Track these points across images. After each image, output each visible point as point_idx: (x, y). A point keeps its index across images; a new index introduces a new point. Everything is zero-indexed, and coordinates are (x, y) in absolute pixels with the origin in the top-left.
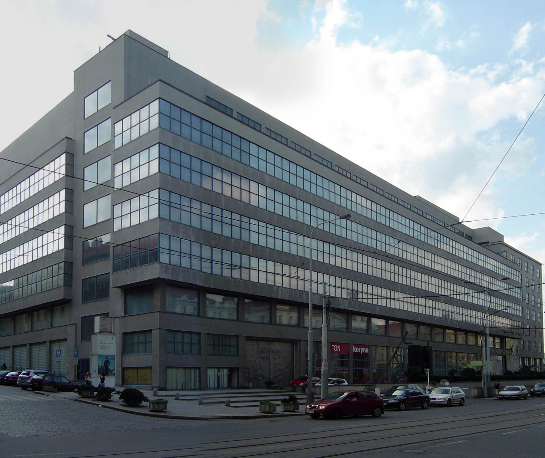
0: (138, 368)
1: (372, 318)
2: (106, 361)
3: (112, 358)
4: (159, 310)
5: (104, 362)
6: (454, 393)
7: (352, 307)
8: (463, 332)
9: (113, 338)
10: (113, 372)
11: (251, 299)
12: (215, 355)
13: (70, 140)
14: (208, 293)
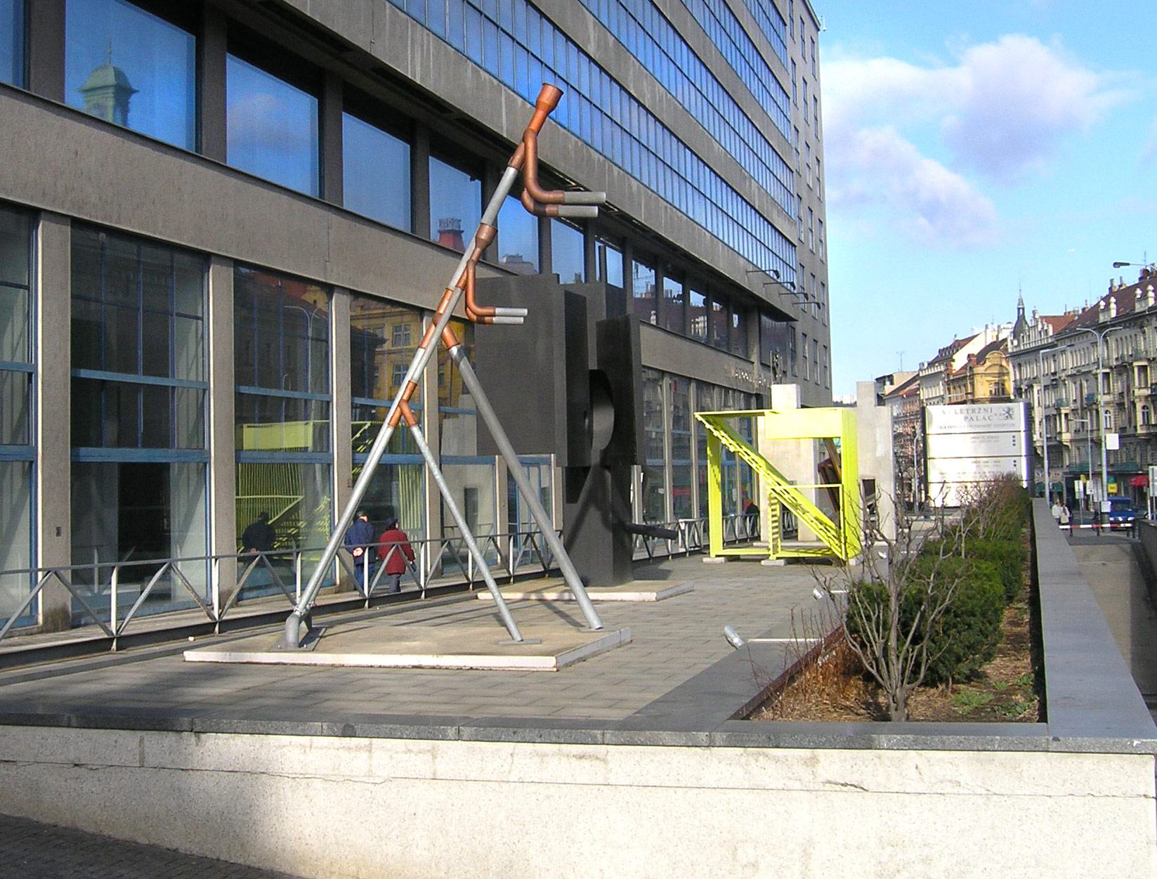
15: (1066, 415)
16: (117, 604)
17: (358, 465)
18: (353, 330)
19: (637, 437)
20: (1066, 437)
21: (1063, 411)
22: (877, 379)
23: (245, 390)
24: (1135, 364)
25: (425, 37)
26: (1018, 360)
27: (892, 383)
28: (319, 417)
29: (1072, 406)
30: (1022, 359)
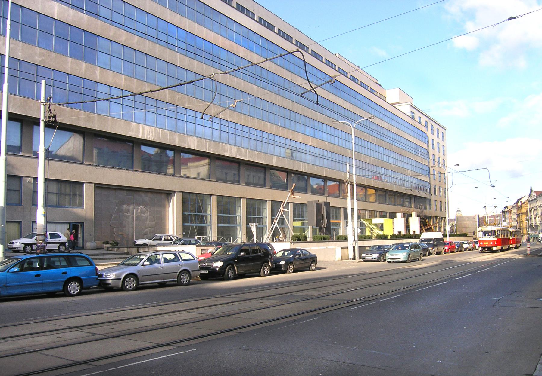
1: (311, 178)
14: (142, 145)
15: (538, 217)
16: (274, 229)
22: (505, 207)
25: (415, 135)
27: (507, 209)
28: (368, 217)
29: (540, 215)
30: (531, 202)
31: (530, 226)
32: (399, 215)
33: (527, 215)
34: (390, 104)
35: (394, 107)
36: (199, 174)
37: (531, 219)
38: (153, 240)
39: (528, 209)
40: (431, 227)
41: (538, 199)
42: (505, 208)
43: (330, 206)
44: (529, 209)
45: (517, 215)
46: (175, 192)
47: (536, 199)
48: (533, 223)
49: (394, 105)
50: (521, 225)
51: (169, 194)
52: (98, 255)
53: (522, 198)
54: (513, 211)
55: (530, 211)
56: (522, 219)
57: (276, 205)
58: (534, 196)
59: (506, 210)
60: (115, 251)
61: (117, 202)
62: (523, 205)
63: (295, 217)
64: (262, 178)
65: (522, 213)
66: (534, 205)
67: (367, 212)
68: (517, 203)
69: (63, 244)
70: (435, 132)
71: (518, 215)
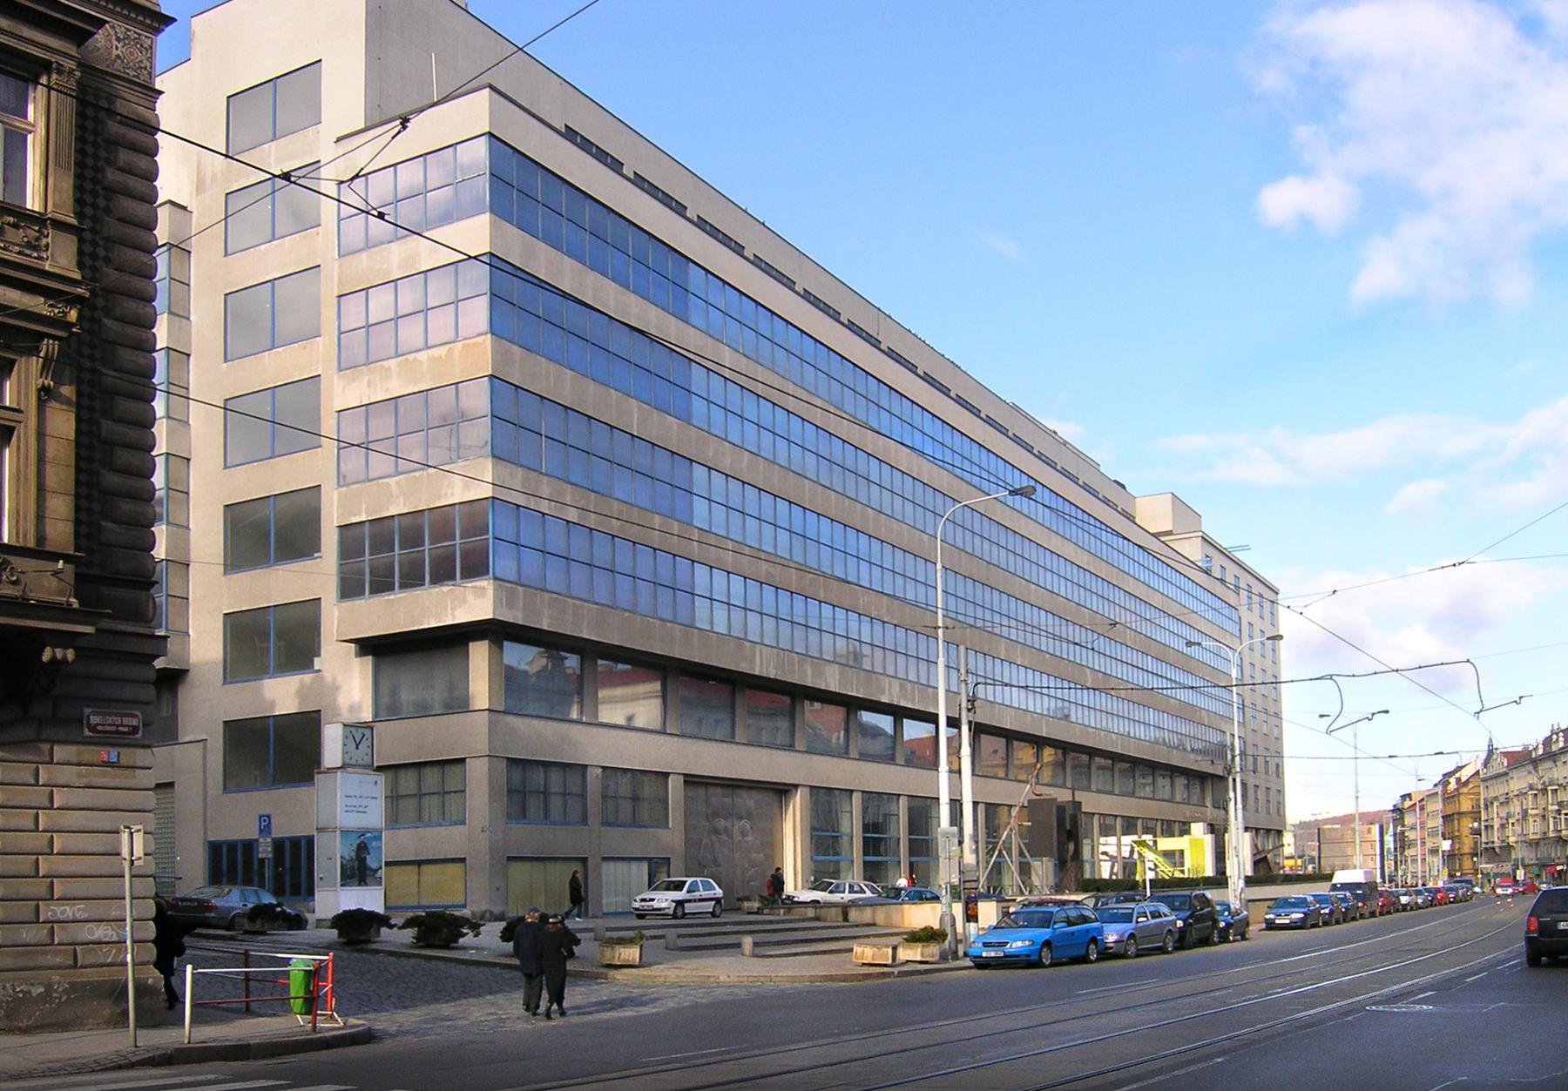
0: (419, 863)
1: (905, 720)
2: (359, 845)
3: (375, 837)
4: (487, 707)
5: (355, 847)
6: (1145, 919)
7: (905, 697)
8: (1128, 762)
9: (376, 783)
10: (378, 875)
11: (628, 664)
12: (619, 826)
13: (181, 212)
14: (508, 640)
15: (1513, 824)
17: (988, 863)
18: (909, 808)
19: (251, 1042)
20: (1512, 840)
21: (1510, 821)
23: (912, 837)
24: (1549, 788)
26: (1487, 784)
27: (1411, 800)
31: (1486, 849)
32: (1198, 828)
33: (1478, 819)
34: (1152, 534)
35: (1163, 542)
36: (630, 718)
37: (1490, 831)
38: (830, 892)
39: (1479, 800)
40: (1266, 857)
41: (1514, 774)
42: (1404, 797)
43: (1083, 810)
44: (1482, 802)
45: (1443, 817)
46: (796, 786)
47: (1506, 774)
48: (1496, 839)
49: (1162, 539)
50: (1457, 846)
51: (783, 791)
52: (750, 923)
53: (1459, 768)
54: (1430, 807)
55: (1486, 807)
56: (1458, 830)
57: (825, 800)
58: (1501, 764)
59: (1408, 803)
60: (779, 915)
61: (709, 812)
62: (1465, 790)
63: (868, 832)
64: (1002, 753)
65: (1459, 813)
66: (1497, 790)
67: (1119, 820)
68: (1444, 781)
69: (718, 900)
70: (1256, 607)
71: (1447, 818)
